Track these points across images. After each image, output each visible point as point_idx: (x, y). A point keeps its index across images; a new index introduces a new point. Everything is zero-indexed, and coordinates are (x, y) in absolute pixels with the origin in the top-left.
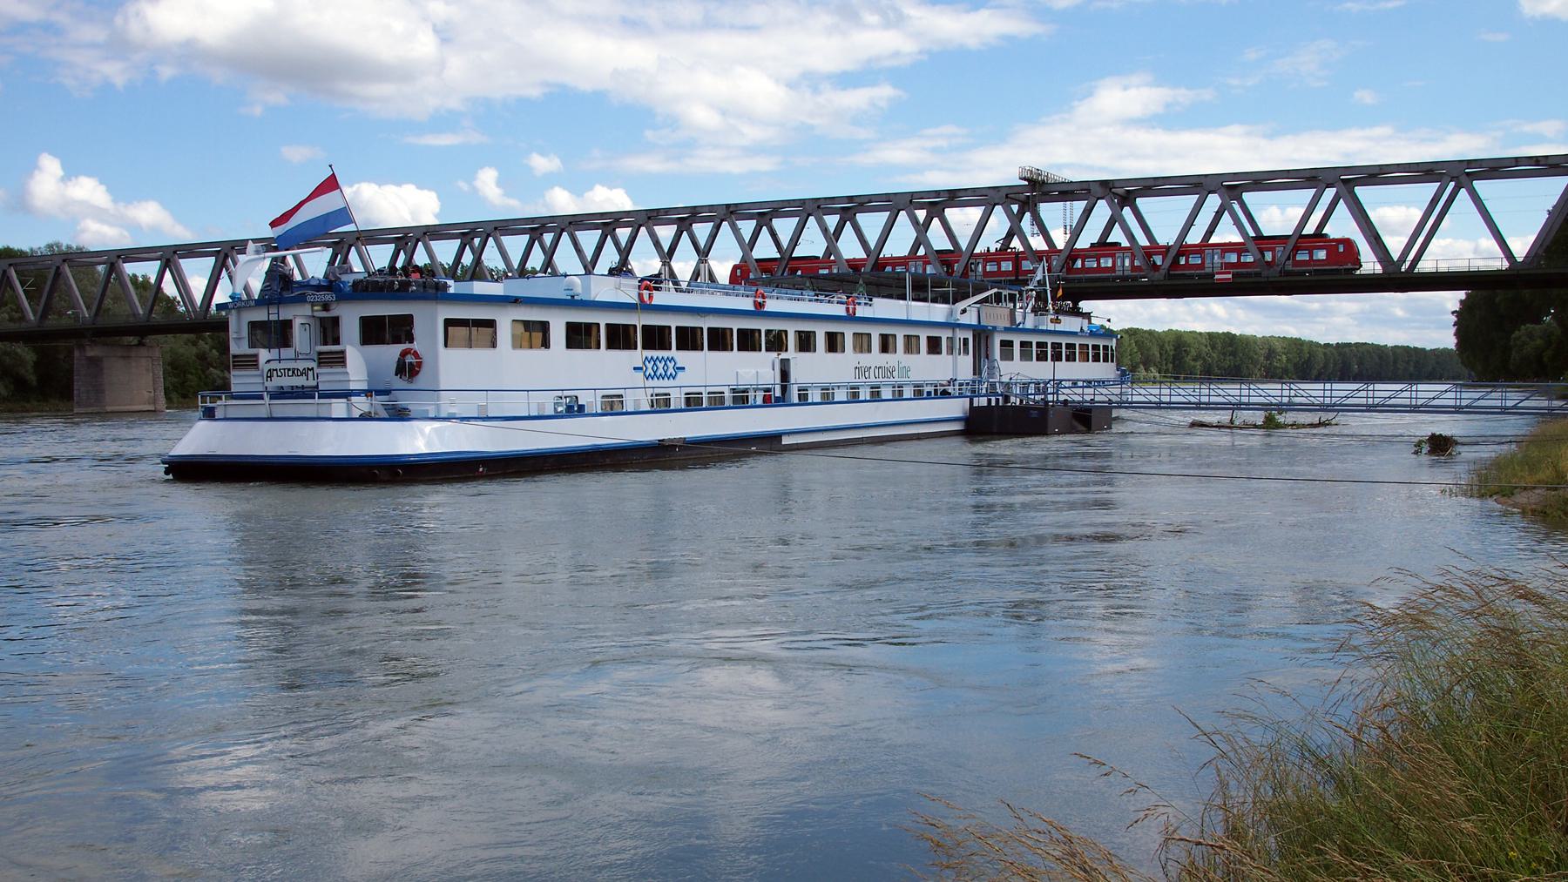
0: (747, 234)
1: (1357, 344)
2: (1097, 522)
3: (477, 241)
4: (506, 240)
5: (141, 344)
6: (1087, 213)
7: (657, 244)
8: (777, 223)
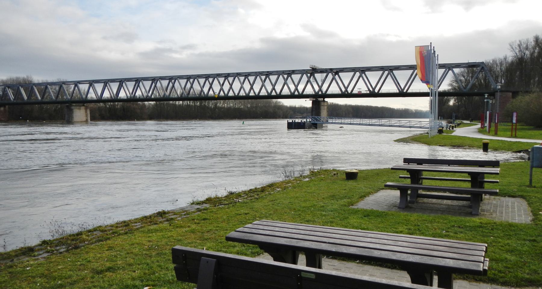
0: (211, 81)
3: (173, 81)
6: (327, 76)
7: (219, 82)
8: (250, 78)
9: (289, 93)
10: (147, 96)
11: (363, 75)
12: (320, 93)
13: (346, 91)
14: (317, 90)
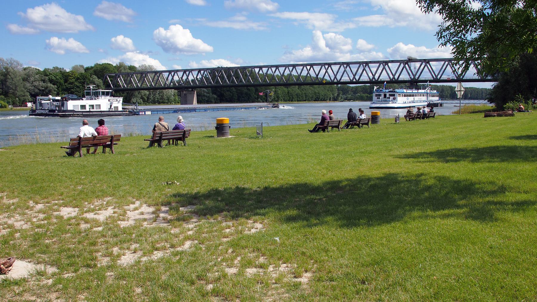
1: (470, 88)
2: (411, 159)
10: (414, 78)
11: (428, 64)
12: (374, 80)
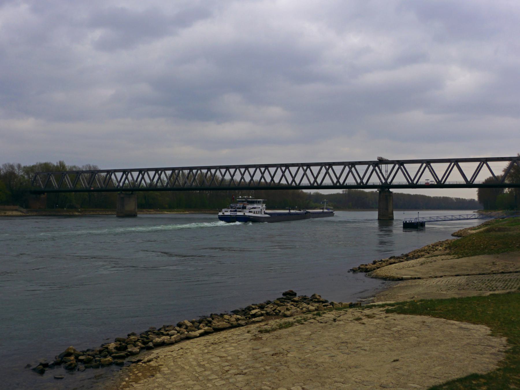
0: (232, 172)
4: (133, 173)
5: (132, 194)
8: (230, 170)
9: (332, 184)
10: (151, 184)
13: (362, 182)
14: (312, 182)
